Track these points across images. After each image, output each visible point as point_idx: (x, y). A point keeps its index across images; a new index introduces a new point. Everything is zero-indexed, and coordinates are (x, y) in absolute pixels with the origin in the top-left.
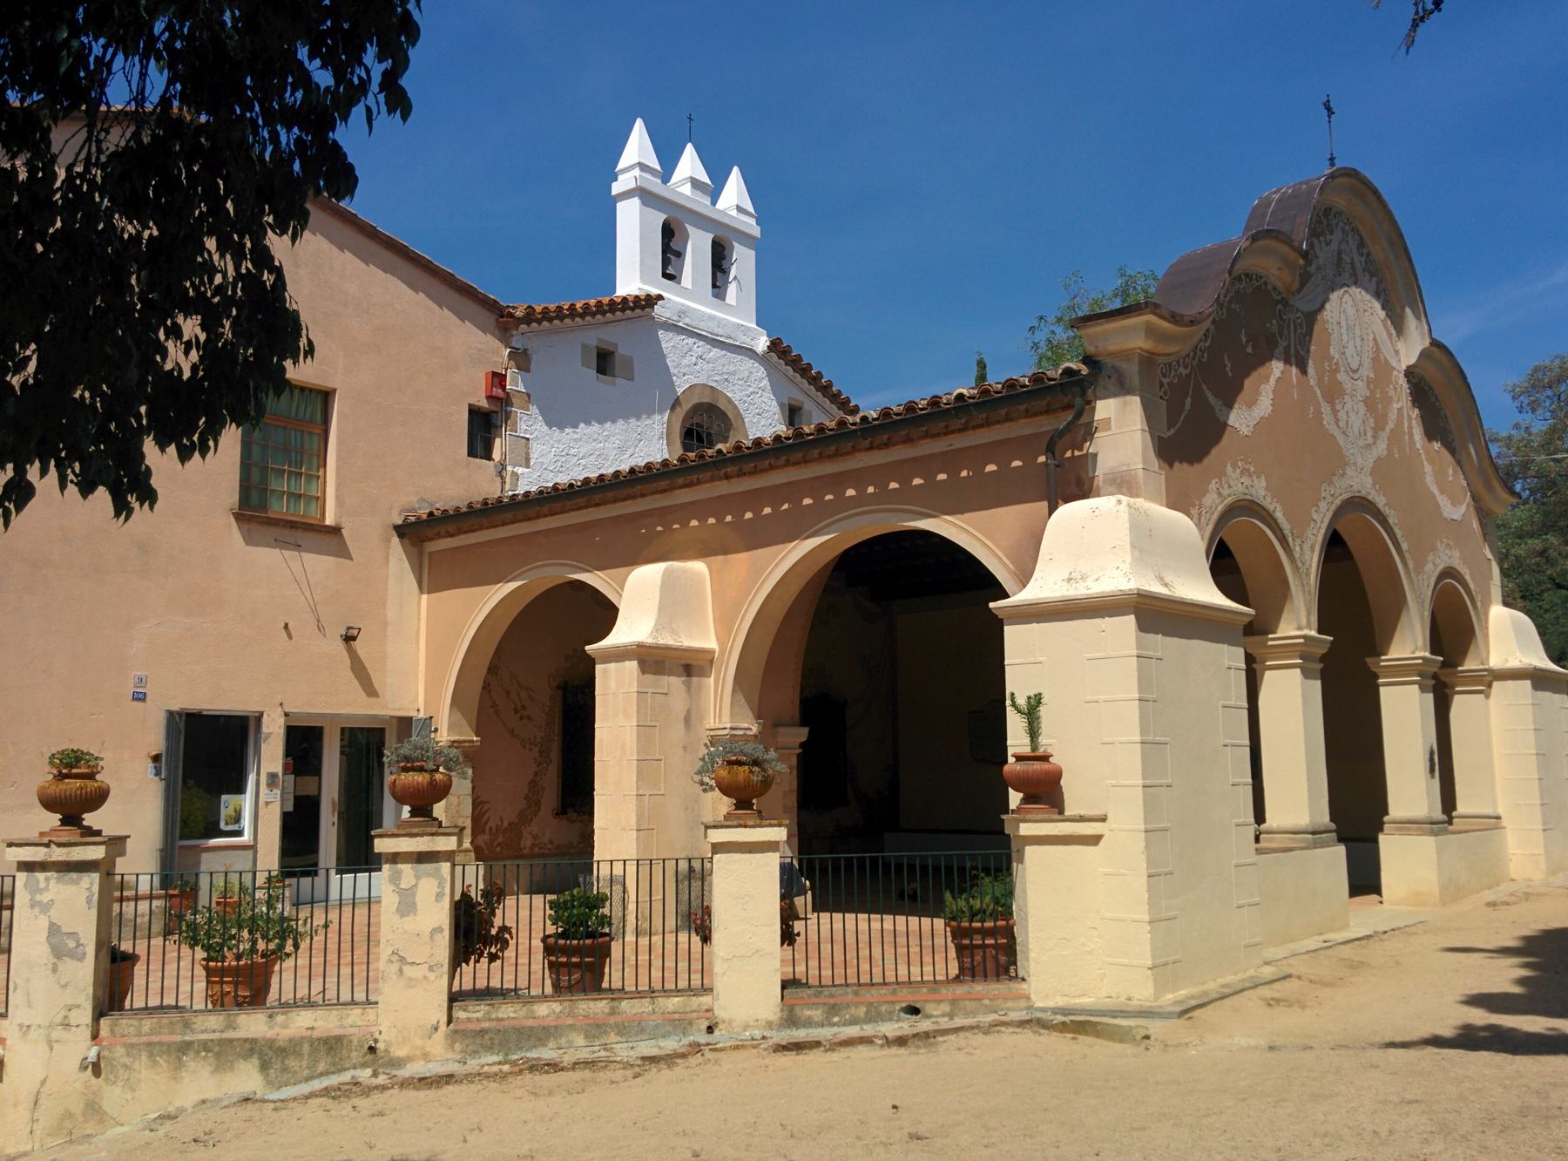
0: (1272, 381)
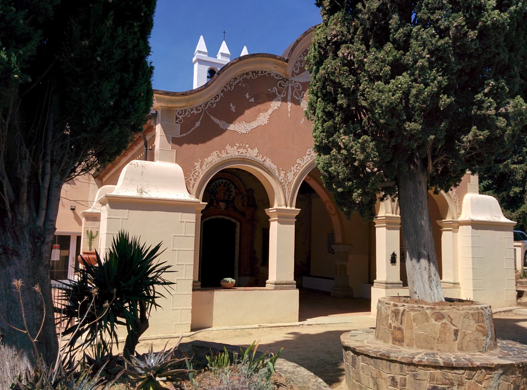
0: (270, 111)
